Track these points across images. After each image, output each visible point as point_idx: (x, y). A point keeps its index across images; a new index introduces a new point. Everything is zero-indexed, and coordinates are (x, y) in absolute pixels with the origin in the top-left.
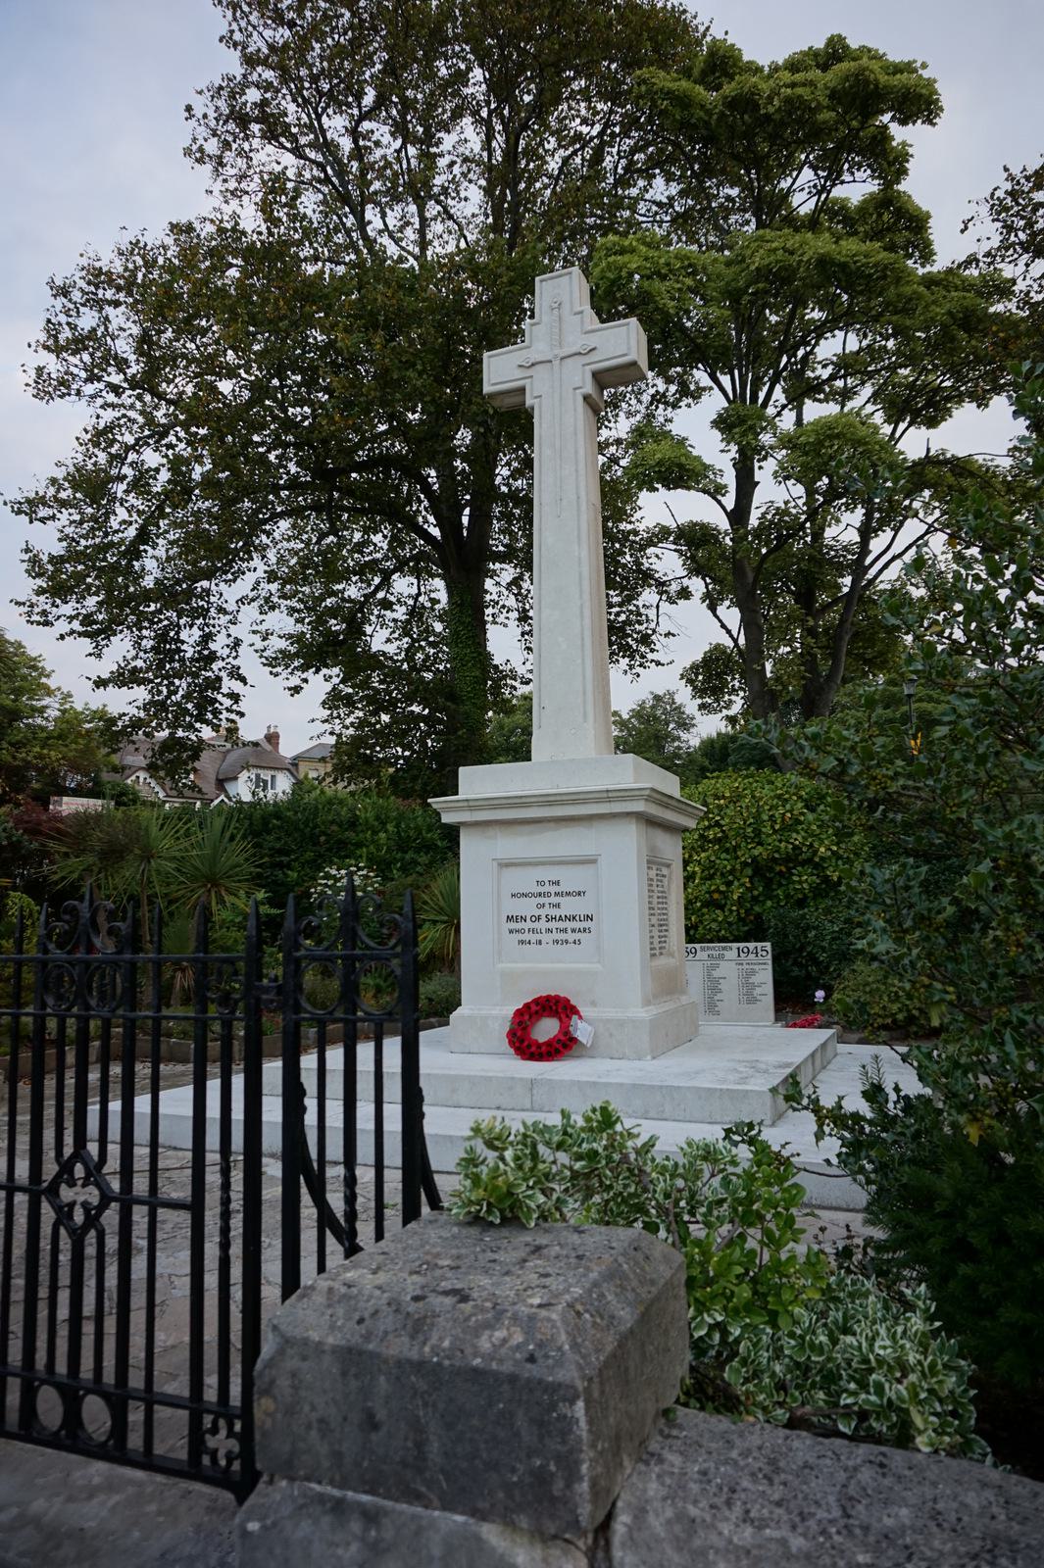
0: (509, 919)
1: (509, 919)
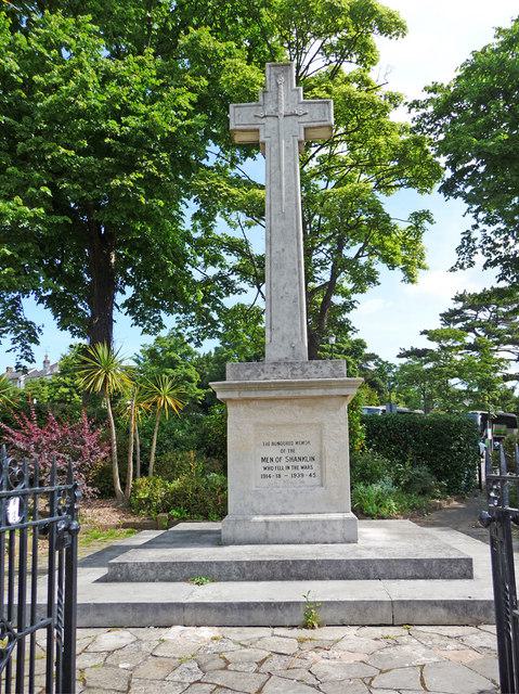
0: (263, 460)
1: (263, 460)
